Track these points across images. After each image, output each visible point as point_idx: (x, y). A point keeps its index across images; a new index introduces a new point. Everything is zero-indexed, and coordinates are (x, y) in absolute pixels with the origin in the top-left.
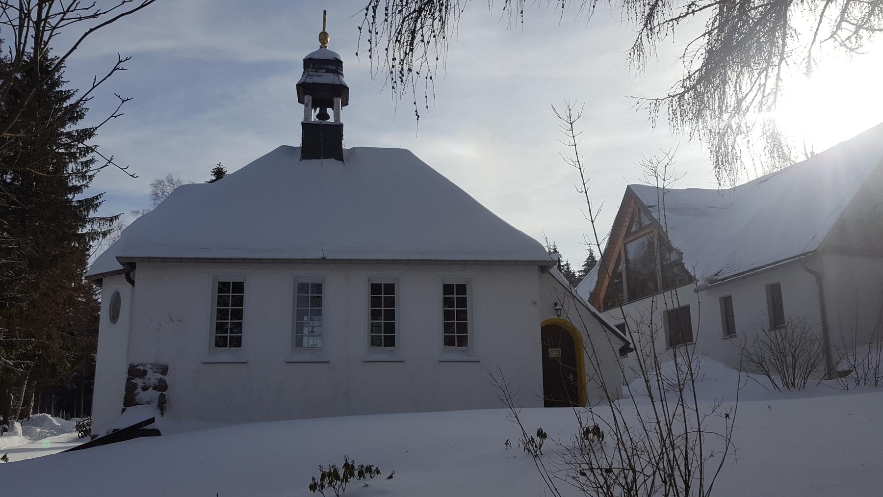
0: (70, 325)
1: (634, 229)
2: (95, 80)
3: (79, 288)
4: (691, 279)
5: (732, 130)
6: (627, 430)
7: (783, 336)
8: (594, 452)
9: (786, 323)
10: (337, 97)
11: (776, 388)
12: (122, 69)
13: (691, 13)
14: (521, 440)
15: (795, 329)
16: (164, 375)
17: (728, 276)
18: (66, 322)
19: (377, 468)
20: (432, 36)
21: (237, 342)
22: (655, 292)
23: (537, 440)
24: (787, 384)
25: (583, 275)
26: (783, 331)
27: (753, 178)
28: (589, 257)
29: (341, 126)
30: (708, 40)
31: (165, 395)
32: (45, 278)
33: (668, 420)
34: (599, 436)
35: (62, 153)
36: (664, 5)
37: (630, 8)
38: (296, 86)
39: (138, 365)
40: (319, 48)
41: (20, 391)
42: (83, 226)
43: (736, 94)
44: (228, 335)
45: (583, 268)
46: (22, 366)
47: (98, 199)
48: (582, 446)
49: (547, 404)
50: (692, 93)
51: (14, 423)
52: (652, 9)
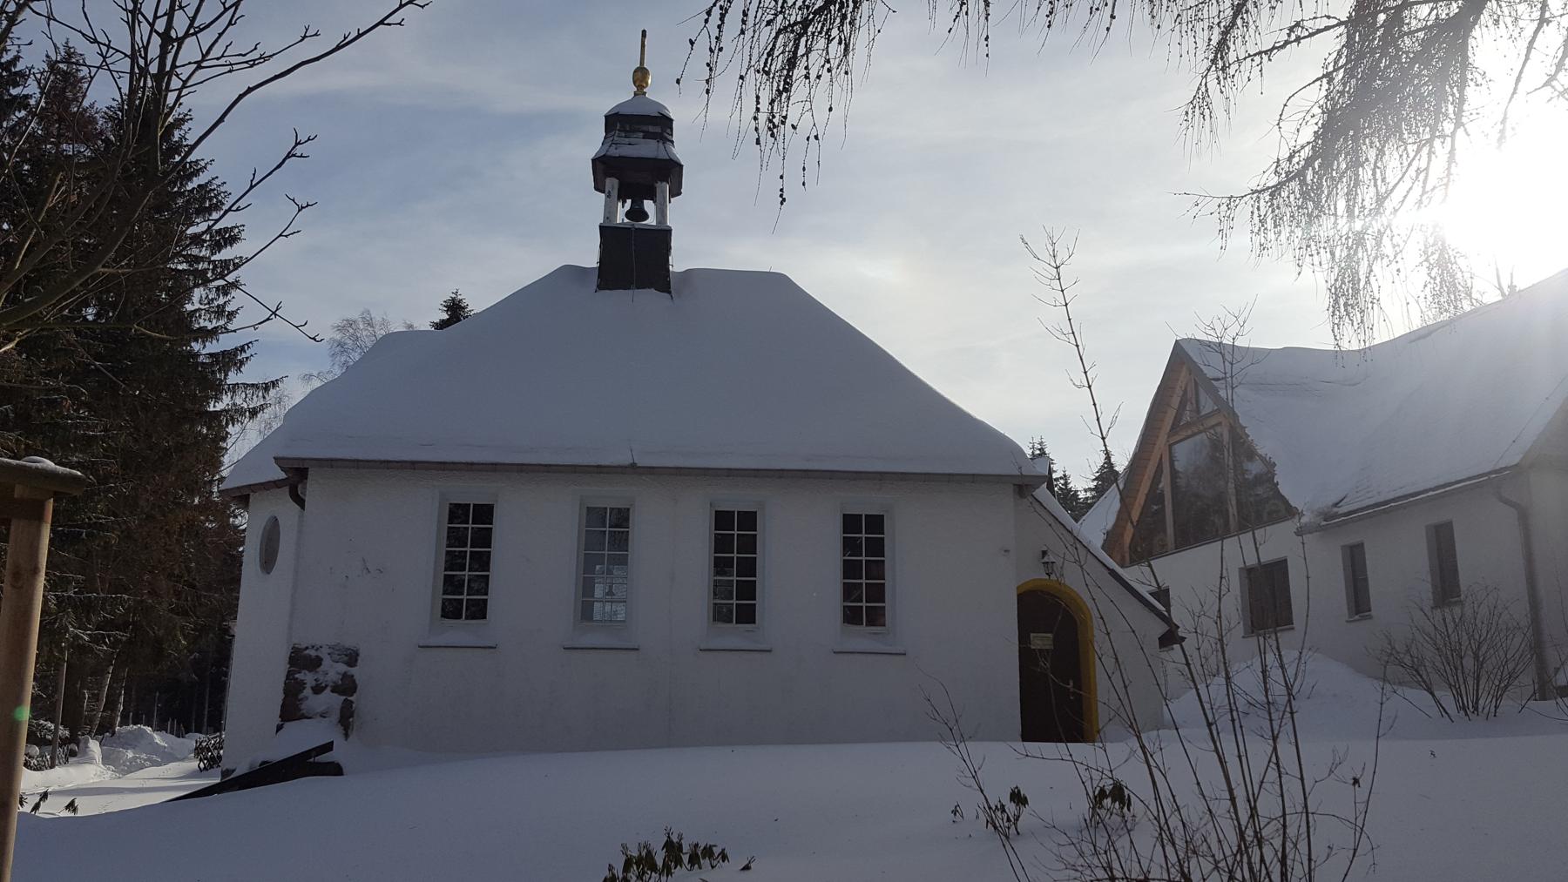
0: (189, 570)
1: (1187, 417)
2: (254, 175)
3: (207, 507)
4: (1291, 512)
5: (1366, 250)
6: (1179, 810)
7: (1457, 621)
8: (1115, 851)
9: (1462, 597)
10: (662, 181)
11: (1444, 713)
12: (301, 156)
13: (1295, 41)
14: (982, 807)
15: (1479, 607)
16: (352, 667)
17: (1359, 507)
18: (183, 565)
19: (723, 850)
20: (826, 68)
21: (479, 611)
22: (1221, 534)
23: (1011, 808)
24: (1464, 708)
25: (1093, 497)
26: (1457, 610)
27: (1400, 331)
28: (1105, 463)
29: (667, 232)
30: (1327, 90)
31: (352, 702)
32: (149, 488)
33: (1250, 793)
34: (1122, 803)
35: (184, 270)
36: (1247, 27)
37: (1184, 34)
38: (591, 162)
39: (307, 648)
40: (633, 95)
41: (101, 689)
42: (218, 399)
43: (1376, 185)
44: (465, 597)
45: (1092, 485)
46: (107, 640)
47: (245, 352)
48: (1091, 820)
49: (1029, 734)
50: (1294, 185)
51: (87, 742)
52: (1226, 33)
